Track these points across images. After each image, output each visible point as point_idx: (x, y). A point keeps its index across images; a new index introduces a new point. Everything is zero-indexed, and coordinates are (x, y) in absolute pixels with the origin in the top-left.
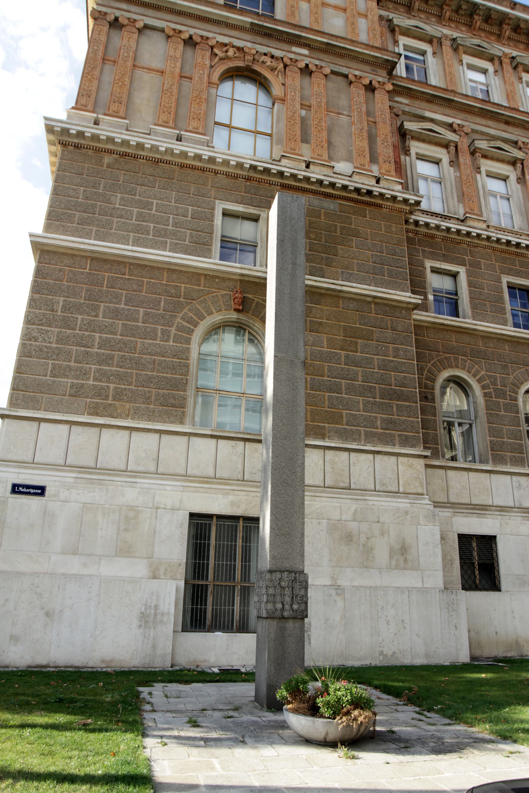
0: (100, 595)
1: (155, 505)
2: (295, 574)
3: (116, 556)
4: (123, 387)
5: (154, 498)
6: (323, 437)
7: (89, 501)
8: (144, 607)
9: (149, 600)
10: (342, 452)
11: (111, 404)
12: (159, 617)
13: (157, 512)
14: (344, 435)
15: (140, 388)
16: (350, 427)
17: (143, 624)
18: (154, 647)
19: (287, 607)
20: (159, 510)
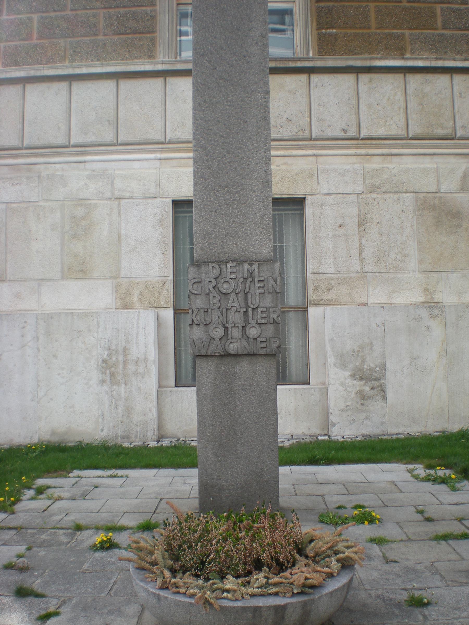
0: (38, 339)
1: (117, 194)
2: (251, 265)
3: (63, 278)
4: (53, 14)
5: (113, 184)
6: (401, 52)
7: (13, 200)
8: (106, 353)
9: (114, 342)
10: (437, 76)
11: (36, 45)
12: (131, 367)
13: (119, 204)
14: (438, 46)
15: (79, 12)
16: (450, 32)
17: (108, 378)
18: (128, 411)
19: (235, 333)
20: (123, 202)
